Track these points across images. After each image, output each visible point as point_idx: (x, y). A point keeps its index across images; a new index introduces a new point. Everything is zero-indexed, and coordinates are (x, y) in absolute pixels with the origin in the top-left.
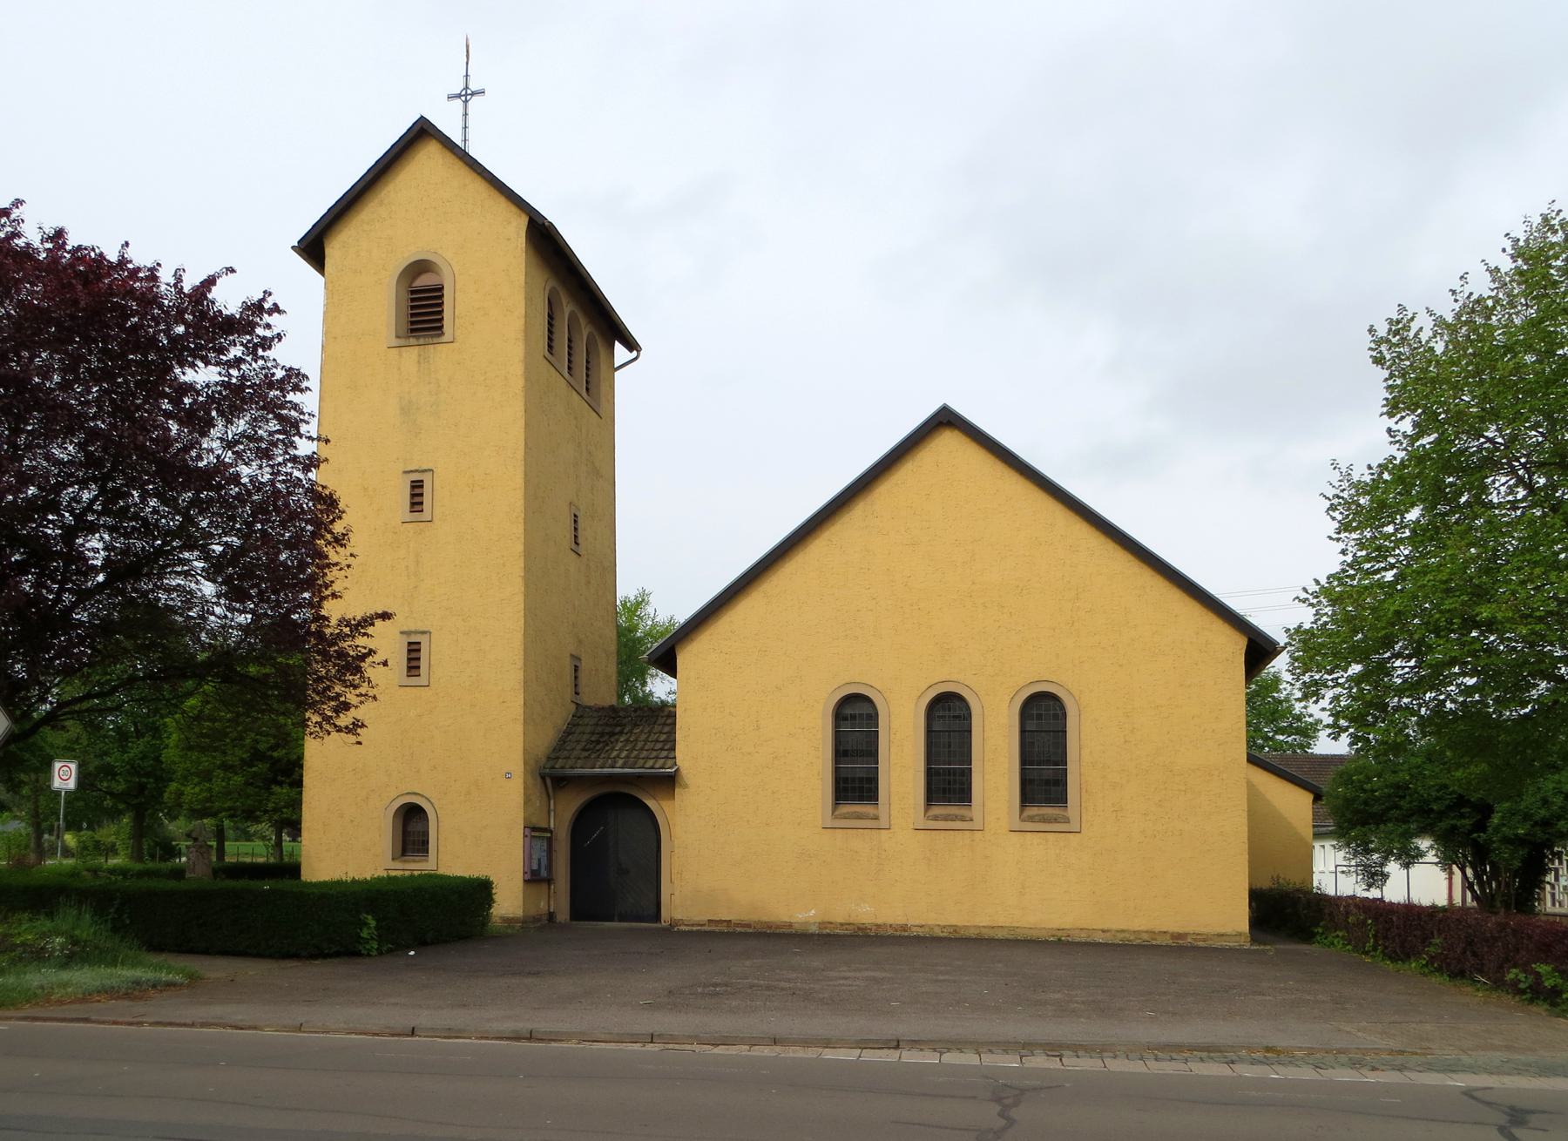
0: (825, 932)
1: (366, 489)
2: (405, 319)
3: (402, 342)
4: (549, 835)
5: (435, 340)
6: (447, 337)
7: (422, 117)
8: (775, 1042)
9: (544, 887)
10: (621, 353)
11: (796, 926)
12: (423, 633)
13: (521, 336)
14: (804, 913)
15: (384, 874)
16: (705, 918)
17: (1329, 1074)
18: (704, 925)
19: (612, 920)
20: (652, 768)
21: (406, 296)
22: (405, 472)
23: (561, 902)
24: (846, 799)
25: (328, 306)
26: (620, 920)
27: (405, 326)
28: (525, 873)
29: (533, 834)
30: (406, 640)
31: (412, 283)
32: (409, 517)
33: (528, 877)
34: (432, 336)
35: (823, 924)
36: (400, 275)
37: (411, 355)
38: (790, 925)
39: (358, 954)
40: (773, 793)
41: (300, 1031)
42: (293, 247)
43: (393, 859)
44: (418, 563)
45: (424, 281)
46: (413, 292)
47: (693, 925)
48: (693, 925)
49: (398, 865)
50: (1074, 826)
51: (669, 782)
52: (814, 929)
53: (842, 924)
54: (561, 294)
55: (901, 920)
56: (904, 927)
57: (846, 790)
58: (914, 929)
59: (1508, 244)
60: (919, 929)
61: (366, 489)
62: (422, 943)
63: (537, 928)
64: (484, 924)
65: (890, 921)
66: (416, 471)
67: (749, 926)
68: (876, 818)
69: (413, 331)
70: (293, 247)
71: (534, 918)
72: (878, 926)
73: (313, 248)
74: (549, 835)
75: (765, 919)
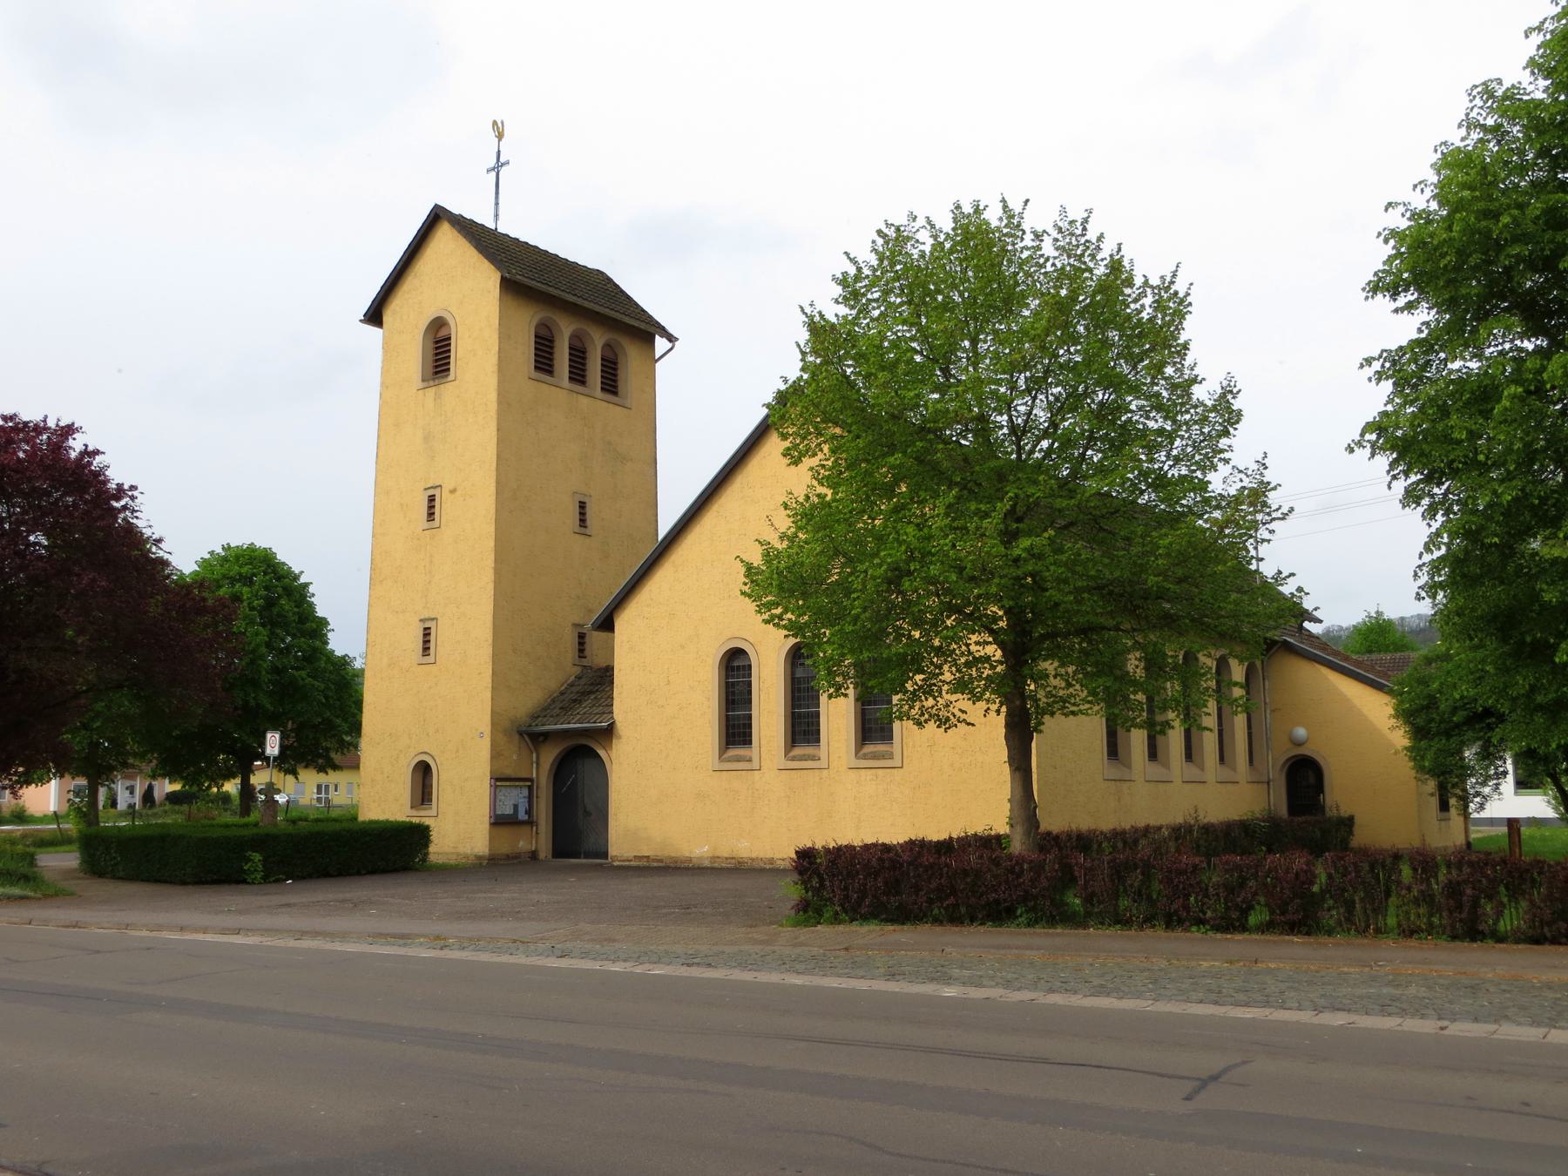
0: (716, 865)
1: (402, 505)
2: (430, 364)
3: (426, 384)
4: (529, 784)
5: (444, 380)
6: (451, 377)
7: (436, 206)
8: (182, 929)
9: (526, 829)
10: (661, 344)
11: (694, 861)
12: (433, 619)
13: (495, 368)
14: (699, 849)
15: (408, 819)
16: (631, 854)
17: (530, 959)
18: (631, 861)
19: (579, 858)
20: (595, 722)
21: (431, 346)
22: (426, 489)
23: (541, 839)
24: (734, 743)
25: (384, 362)
26: (586, 857)
27: (431, 370)
28: (491, 817)
29: (498, 783)
30: (422, 626)
31: (438, 331)
32: (427, 525)
33: (492, 820)
34: (442, 377)
35: (714, 858)
36: (427, 328)
37: (431, 392)
38: (690, 860)
39: (244, 882)
40: (679, 741)
41: (30, 924)
42: (361, 321)
43: (412, 807)
44: (431, 562)
45: (443, 333)
46: (437, 342)
47: (624, 861)
48: (624, 861)
49: (415, 813)
50: (755, 765)
51: (608, 732)
52: (707, 863)
53: (726, 858)
54: (555, 317)
55: (769, 855)
56: (771, 861)
57: (734, 735)
58: (778, 862)
59: (1077, 214)
60: (782, 863)
61: (402, 505)
62: (296, 878)
63: (495, 866)
64: (424, 860)
65: (762, 855)
66: (432, 487)
67: (661, 861)
68: (750, 760)
69: (436, 373)
70: (361, 321)
71: (508, 856)
72: (753, 859)
73: (374, 316)
74: (529, 784)
75: (673, 855)
